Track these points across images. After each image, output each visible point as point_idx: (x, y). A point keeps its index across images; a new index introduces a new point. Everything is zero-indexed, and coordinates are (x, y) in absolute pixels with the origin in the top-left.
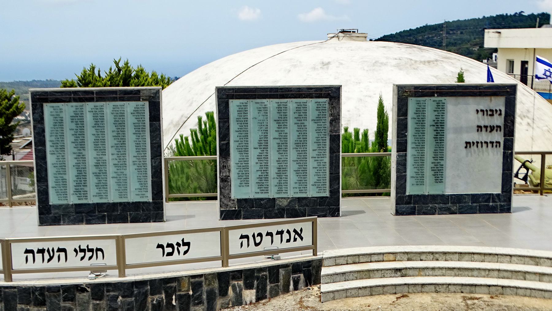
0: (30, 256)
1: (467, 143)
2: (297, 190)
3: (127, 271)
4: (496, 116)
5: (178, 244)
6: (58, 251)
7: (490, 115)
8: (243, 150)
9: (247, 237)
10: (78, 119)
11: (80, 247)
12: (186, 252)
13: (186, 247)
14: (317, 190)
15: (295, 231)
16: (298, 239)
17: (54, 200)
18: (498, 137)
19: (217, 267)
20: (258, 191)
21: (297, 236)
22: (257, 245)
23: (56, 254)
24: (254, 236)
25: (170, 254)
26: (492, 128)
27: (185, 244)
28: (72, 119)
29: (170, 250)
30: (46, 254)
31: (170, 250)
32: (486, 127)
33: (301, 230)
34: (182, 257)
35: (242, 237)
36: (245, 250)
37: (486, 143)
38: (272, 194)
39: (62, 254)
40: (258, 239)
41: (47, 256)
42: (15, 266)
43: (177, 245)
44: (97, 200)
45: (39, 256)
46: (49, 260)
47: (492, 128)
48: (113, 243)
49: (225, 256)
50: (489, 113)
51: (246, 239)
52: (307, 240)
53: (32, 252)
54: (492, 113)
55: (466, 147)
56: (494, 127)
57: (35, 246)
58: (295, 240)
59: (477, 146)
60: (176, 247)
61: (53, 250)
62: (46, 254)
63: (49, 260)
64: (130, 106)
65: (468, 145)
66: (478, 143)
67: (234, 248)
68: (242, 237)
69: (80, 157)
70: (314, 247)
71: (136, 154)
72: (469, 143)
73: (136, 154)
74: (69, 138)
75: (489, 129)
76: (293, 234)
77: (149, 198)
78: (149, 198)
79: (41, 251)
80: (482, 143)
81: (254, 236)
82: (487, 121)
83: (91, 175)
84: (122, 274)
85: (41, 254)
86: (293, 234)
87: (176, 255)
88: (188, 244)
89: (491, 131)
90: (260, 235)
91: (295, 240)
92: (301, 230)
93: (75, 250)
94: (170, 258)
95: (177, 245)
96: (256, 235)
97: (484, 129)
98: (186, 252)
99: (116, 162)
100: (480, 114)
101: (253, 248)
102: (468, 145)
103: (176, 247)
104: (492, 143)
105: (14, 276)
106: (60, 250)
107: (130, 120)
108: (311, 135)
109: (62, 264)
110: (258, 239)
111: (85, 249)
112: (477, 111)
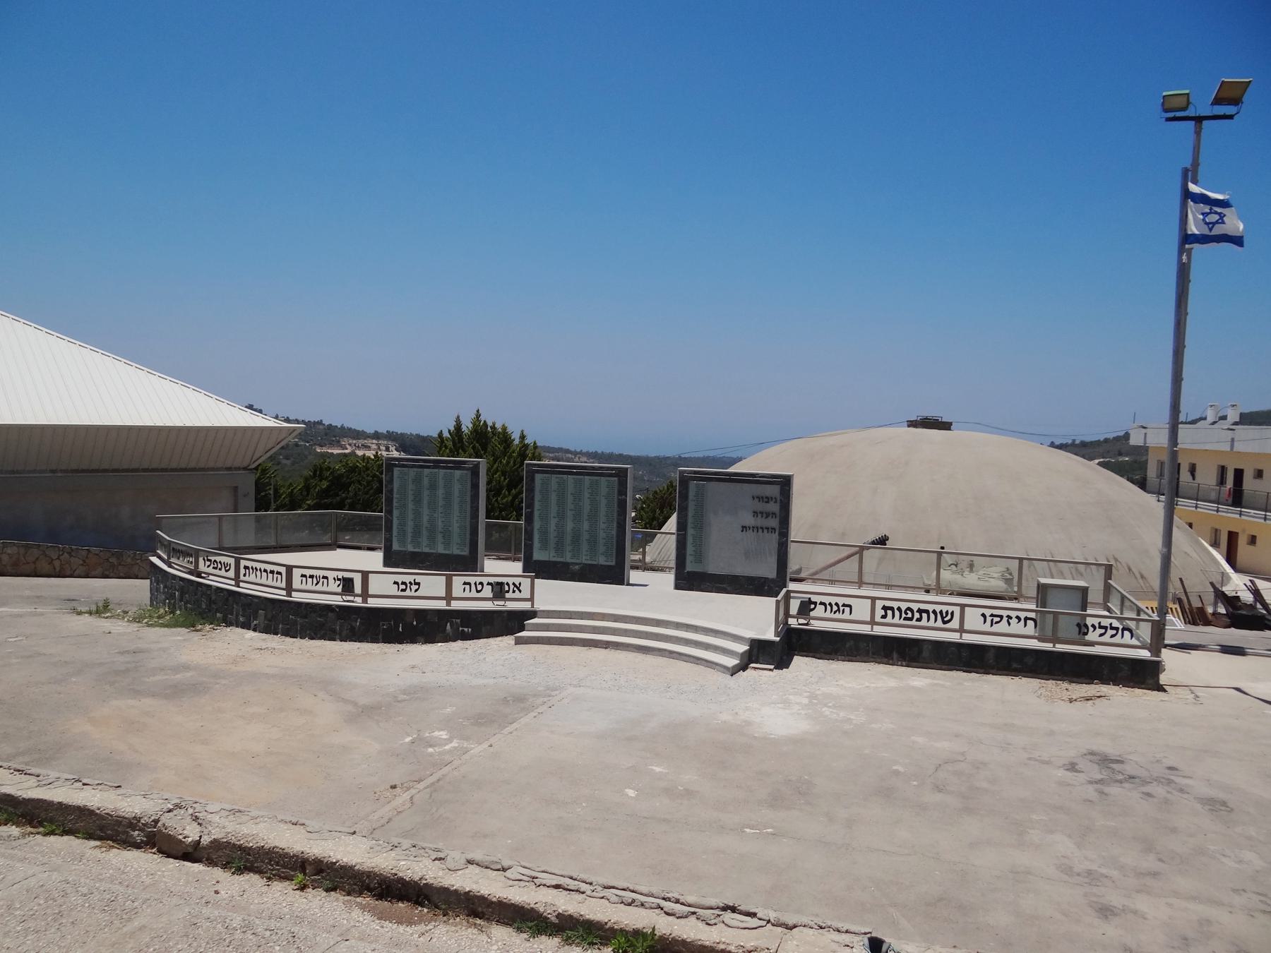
0: (304, 579)
1: (743, 527)
2: (588, 558)
3: (294, 594)
4: (772, 503)
5: (410, 583)
6: (842, 606)
7: (766, 502)
8: (545, 518)
9: (469, 584)
10: (418, 480)
11: (415, 580)
12: (416, 591)
13: (417, 587)
14: (605, 559)
15: (514, 584)
16: (517, 591)
17: (396, 546)
18: (774, 523)
19: (441, 605)
20: (555, 555)
21: (515, 589)
22: (478, 591)
23: (322, 580)
24: (475, 584)
25: (403, 590)
26: (768, 515)
27: (416, 584)
28: (414, 481)
29: (404, 587)
30: (315, 579)
31: (404, 587)
32: (762, 513)
33: (520, 584)
34: (413, 594)
35: (465, 583)
36: (467, 594)
37: (762, 528)
38: (568, 558)
39: (325, 580)
40: (479, 587)
41: (315, 582)
42: (294, 586)
43: (897, 609)
44: (426, 550)
45: (310, 580)
46: (316, 584)
47: (768, 515)
48: (959, 608)
49: (449, 597)
50: (765, 500)
51: (468, 586)
52: (526, 593)
53: (305, 576)
54: (767, 500)
55: (742, 531)
56: (769, 513)
57: (308, 572)
58: (514, 592)
59: (753, 531)
60: (409, 585)
61: (319, 577)
62: (315, 579)
63: (316, 584)
64: (458, 473)
65: (745, 529)
66: (753, 527)
67: (457, 590)
68: (465, 583)
69: (418, 514)
70: (531, 599)
71: (459, 515)
72: (745, 527)
73: (459, 515)
74: (554, 509)
75: (765, 515)
76: (512, 587)
77: (466, 552)
78: (466, 552)
79: (311, 577)
80: (757, 528)
81: (475, 584)
82: (761, 507)
83: (424, 529)
84: (365, 601)
85: (311, 579)
86: (512, 587)
87: (408, 593)
88: (418, 584)
89: (766, 517)
90: (481, 583)
91: (514, 592)
92: (520, 584)
93: (334, 579)
94: (403, 593)
95: (897, 609)
96: (477, 583)
97: (760, 516)
98: (416, 591)
99: (443, 519)
100: (757, 500)
101: (474, 594)
102: (745, 529)
103: (409, 585)
104: (768, 529)
105: (294, 594)
106: (324, 577)
107: (456, 488)
108: (603, 510)
109: (325, 588)
110: (479, 587)
111: (1107, 627)
112: (753, 498)
